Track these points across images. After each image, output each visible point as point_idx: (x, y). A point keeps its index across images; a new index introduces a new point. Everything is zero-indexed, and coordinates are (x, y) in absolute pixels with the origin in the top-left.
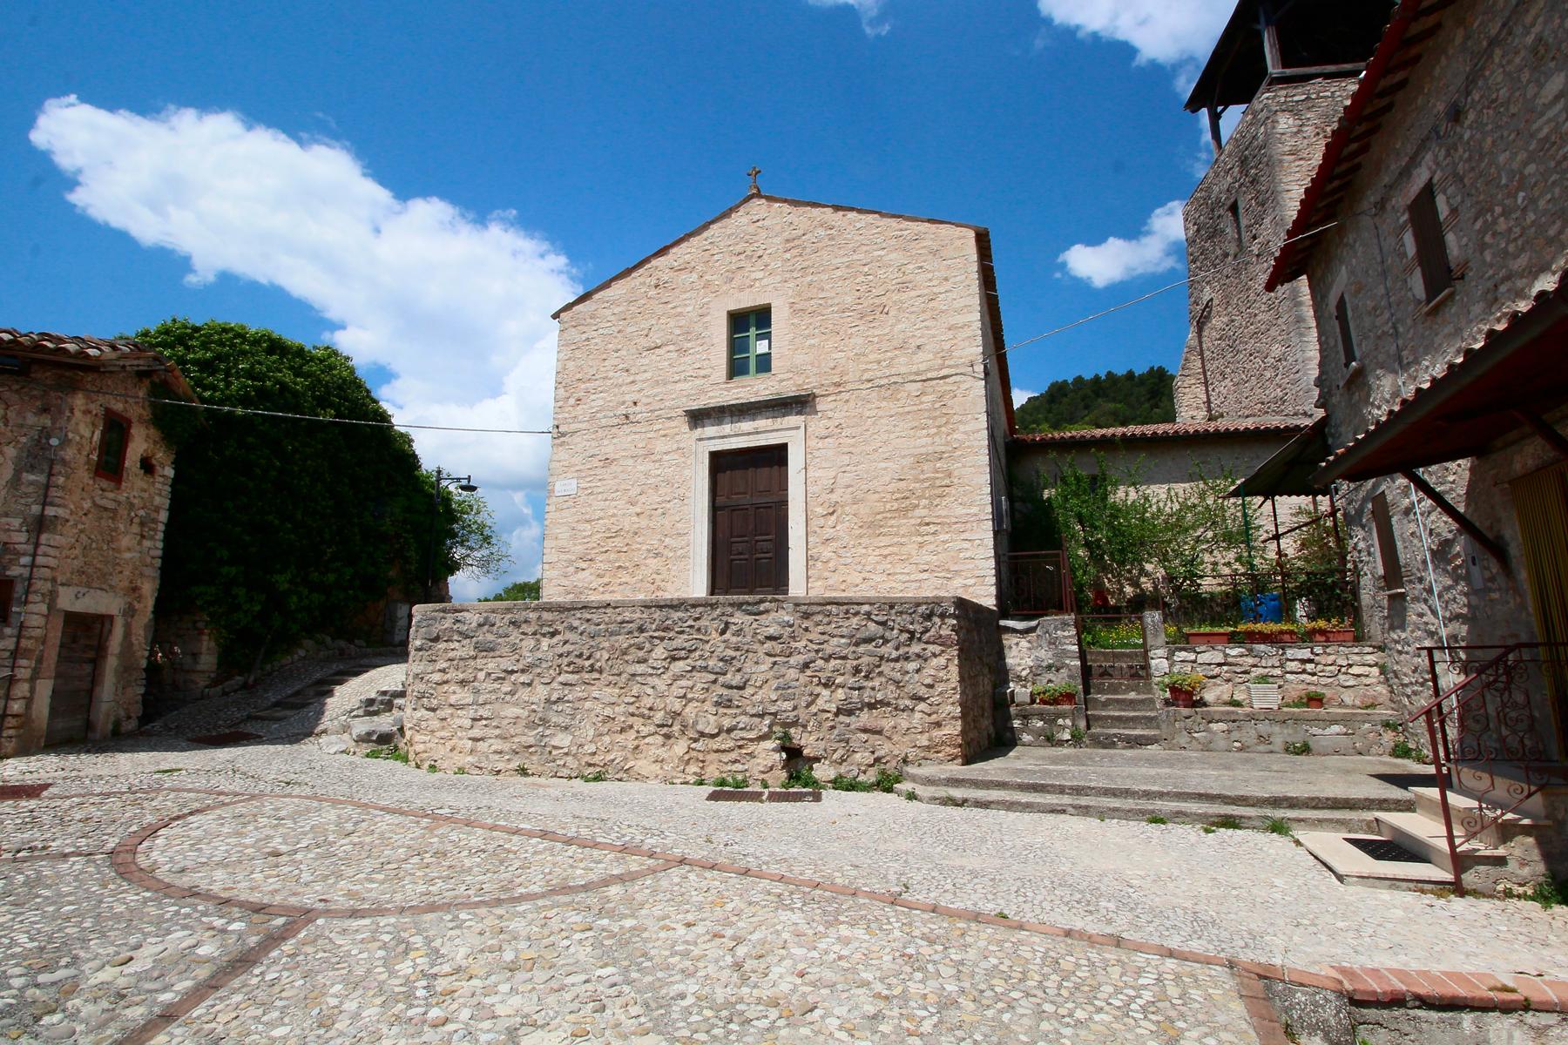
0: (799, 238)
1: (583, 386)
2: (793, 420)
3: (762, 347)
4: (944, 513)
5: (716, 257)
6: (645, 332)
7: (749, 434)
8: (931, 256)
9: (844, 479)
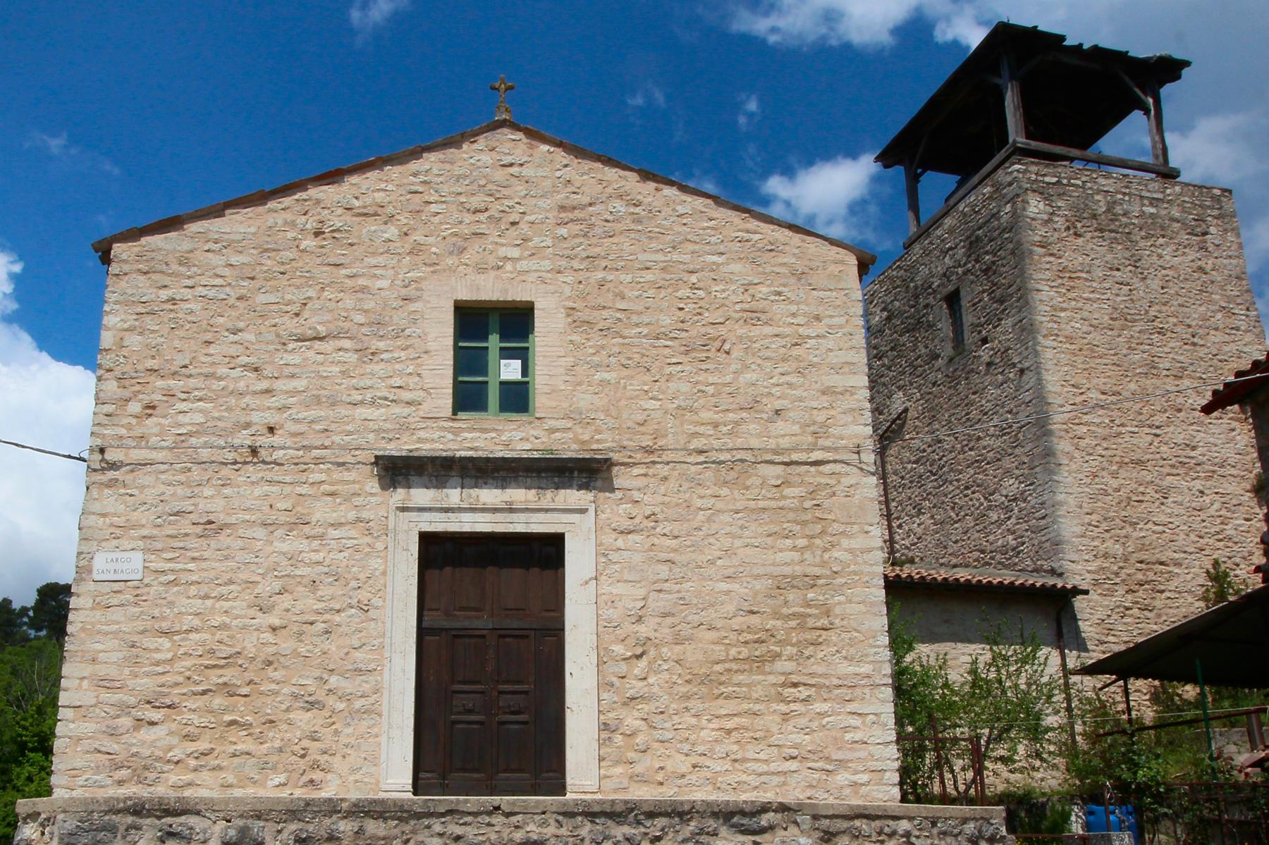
0: (582, 207)
1: (160, 383)
2: (573, 497)
3: (510, 370)
4: (820, 669)
5: (434, 208)
6: (295, 308)
7: (495, 510)
8: (793, 280)
9: (658, 603)
